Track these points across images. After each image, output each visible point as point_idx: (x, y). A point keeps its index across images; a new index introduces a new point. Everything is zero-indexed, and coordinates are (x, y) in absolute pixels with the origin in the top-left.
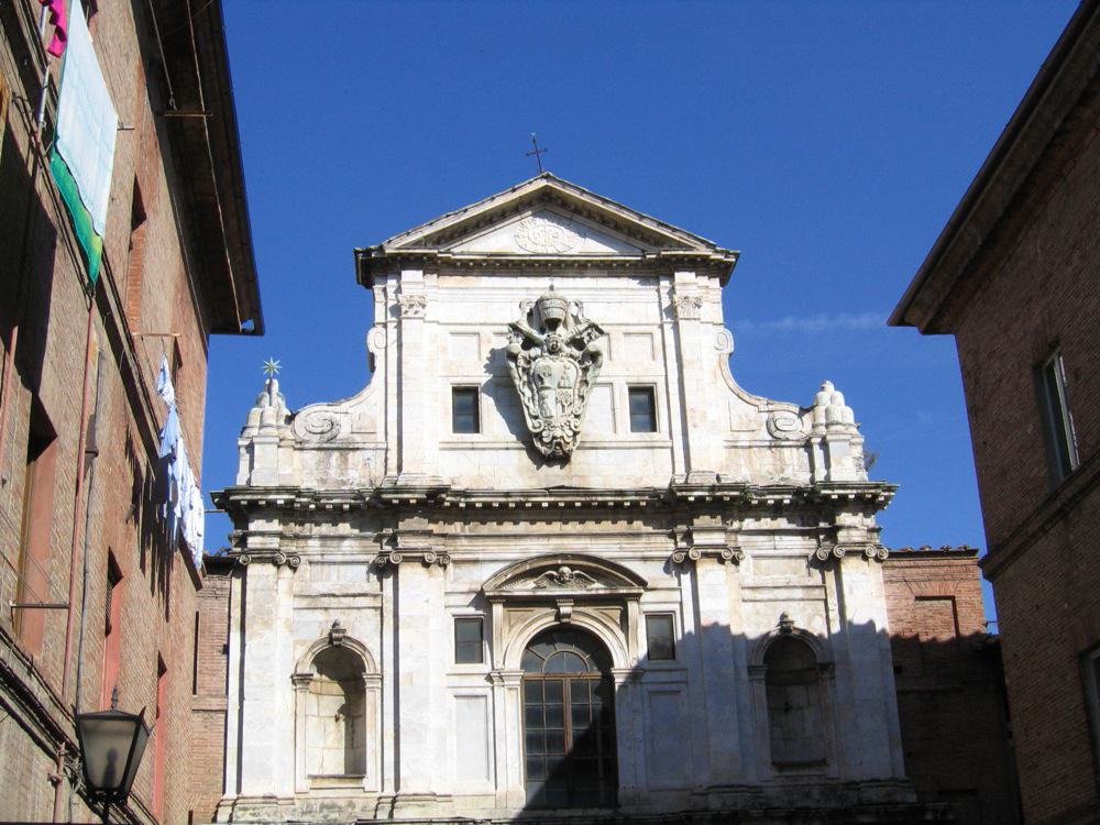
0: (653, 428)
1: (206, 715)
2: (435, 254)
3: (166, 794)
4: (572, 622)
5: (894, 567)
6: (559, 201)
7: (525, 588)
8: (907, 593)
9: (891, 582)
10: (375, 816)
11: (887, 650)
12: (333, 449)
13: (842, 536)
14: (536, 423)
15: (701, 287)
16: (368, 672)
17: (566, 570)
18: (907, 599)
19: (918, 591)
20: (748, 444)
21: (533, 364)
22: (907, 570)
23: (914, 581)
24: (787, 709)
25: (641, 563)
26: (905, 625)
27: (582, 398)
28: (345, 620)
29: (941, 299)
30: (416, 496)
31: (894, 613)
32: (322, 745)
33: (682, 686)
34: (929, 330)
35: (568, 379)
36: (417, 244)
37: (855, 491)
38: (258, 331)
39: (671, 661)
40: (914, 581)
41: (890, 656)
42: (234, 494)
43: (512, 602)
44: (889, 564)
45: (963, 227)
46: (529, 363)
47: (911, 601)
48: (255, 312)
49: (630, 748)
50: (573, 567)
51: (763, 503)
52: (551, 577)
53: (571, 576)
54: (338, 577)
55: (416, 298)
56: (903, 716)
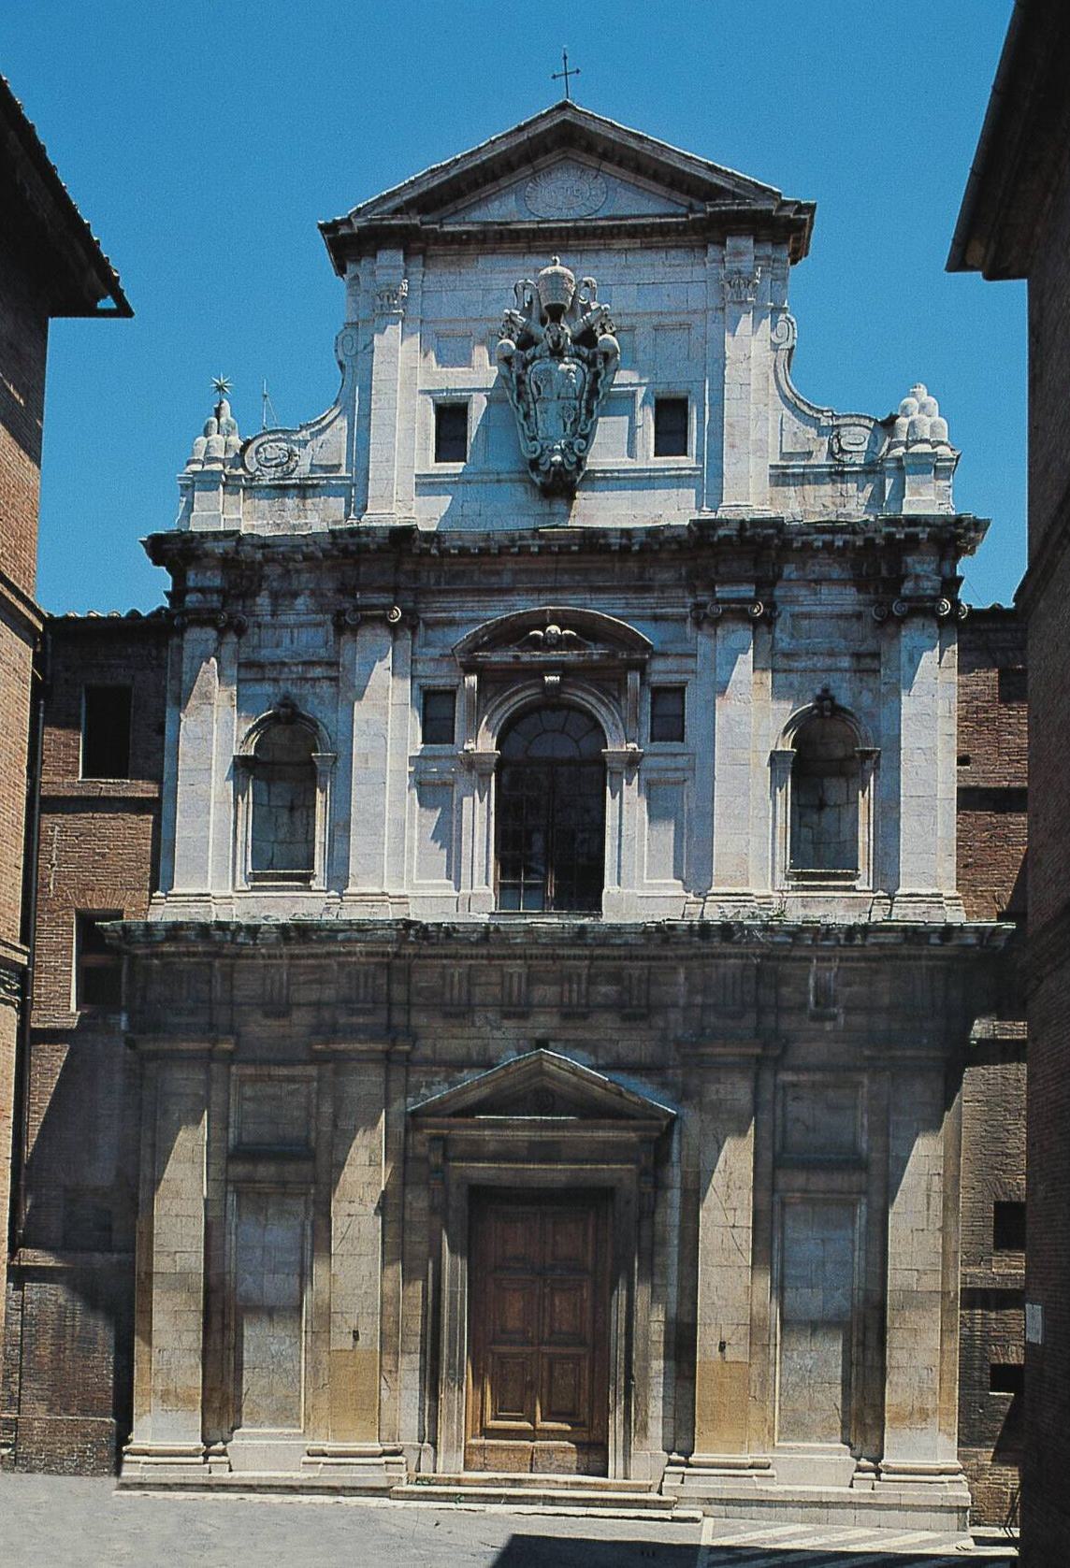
6: (583, 143)
10: (808, 1179)
13: (907, 588)
24: (821, 806)
25: (650, 626)
32: (272, 839)
39: (680, 743)
48: (113, 287)
51: (807, 546)
54: (292, 642)
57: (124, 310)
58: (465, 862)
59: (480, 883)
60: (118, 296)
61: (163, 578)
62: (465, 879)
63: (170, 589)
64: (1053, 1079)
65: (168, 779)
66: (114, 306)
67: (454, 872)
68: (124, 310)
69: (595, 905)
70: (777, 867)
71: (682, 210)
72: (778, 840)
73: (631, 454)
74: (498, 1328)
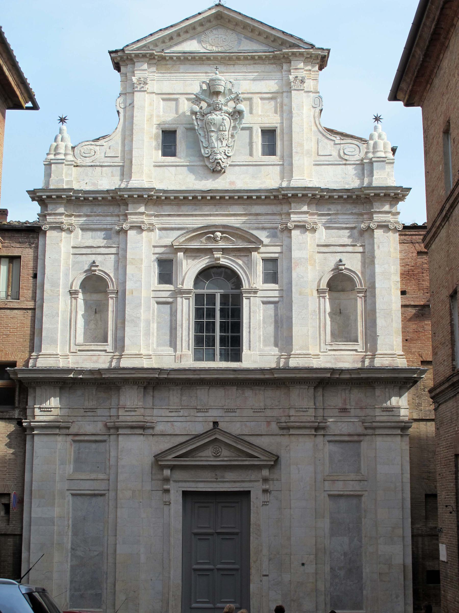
0: (248, 493)
3: (438, 429)
5: (406, 235)
7: (195, 245)
8: (413, 250)
9: (404, 243)
15: (306, 70)
16: (244, 288)
17: (219, 234)
18: (412, 253)
21: (205, 117)
22: (414, 237)
23: (417, 242)
26: (410, 268)
27: (233, 136)
28: (99, 259)
29: (410, 87)
31: (404, 261)
34: (408, 104)
35: (225, 126)
37: (384, 191)
38: (329, 50)
40: (417, 242)
42: (38, 192)
43: (186, 251)
44: (403, 233)
45: (413, 50)
47: (415, 254)
48: (30, 97)
50: (222, 233)
53: (221, 238)
55: (142, 79)
57: (35, 107)
58: (179, 340)
59: (185, 349)
60: (34, 102)
61: (36, 208)
62: (179, 347)
63: (39, 212)
64: (446, 447)
65: (38, 300)
66: (32, 106)
67: (173, 343)
68: (35, 107)
69: (237, 357)
70: (322, 341)
71: (271, 50)
72: (322, 329)
73: (251, 154)
74: (444, 568)
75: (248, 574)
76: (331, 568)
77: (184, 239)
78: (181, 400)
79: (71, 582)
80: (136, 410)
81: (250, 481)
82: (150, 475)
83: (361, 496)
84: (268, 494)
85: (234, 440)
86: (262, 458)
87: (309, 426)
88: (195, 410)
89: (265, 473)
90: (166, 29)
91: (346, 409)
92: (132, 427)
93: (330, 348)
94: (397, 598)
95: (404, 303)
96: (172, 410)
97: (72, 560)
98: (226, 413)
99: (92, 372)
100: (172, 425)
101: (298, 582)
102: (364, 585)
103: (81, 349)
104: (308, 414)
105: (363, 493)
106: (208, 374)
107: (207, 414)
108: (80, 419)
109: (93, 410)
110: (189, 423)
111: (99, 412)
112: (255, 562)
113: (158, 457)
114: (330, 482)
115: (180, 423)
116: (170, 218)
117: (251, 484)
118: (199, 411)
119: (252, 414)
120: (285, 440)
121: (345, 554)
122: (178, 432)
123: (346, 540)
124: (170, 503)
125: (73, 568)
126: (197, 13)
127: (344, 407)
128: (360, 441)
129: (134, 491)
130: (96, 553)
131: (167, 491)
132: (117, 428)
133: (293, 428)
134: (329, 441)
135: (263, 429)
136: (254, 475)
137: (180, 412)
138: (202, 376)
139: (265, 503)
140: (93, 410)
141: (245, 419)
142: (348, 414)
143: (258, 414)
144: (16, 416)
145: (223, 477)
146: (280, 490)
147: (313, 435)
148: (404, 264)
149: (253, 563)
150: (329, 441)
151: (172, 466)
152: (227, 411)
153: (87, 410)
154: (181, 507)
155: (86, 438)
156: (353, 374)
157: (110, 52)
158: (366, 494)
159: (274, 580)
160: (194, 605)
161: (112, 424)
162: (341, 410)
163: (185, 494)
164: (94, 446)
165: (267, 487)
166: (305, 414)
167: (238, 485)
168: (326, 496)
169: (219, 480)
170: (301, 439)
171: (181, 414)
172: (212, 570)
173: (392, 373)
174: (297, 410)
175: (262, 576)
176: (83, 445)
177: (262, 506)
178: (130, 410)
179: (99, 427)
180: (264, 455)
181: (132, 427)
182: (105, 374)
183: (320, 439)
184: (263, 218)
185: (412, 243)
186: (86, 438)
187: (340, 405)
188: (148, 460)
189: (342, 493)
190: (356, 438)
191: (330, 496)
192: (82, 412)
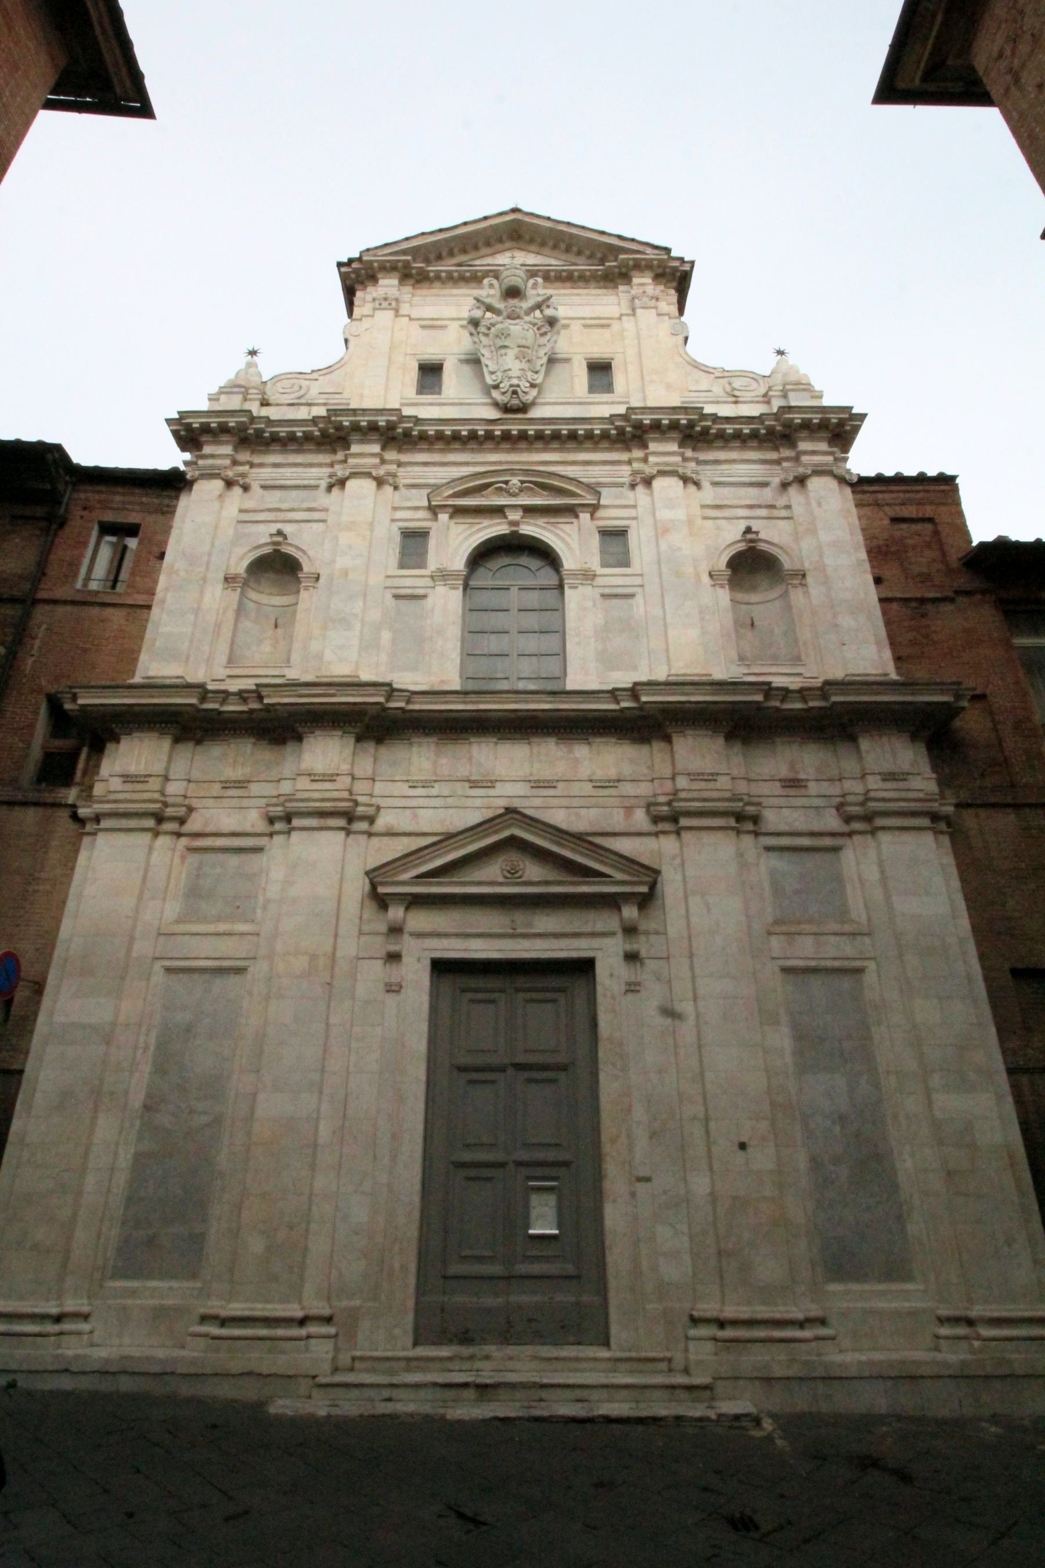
0: (585, 967)
1: (129, 610)
2: (408, 262)
4: (521, 532)
5: (864, 492)
11: (864, 560)
12: (301, 404)
14: (494, 377)
18: (881, 520)
19: (891, 512)
20: (313, 1329)
22: (880, 496)
23: (887, 504)
30: (367, 418)
33: (639, 590)
36: (391, 254)
37: (819, 416)
38: (692, 263)
41: (867, 566)
46: (489, 329)
49: (579, 644)
52: (500, 489)
56: (888, 623)
75: (599, 1176)
76: (813, 1159)
77: (451, 492)
78: (435, 763)
79: (130, 1201)
80: (335, 778)
81: (593, 935)
82: (357, 921)
83: (860, 971)
84: (638, 964)
85: (554, 838)
86: (619, 876)
87: (721, 809)
88: (467, 785)
89: (630, 912)
90: (432, 233)
91: (798, 780)
92: (322, 814)
93: (746, 671)
94: (1009, 1246)
95: (883, 595)
96: (415, 784)
97: (140, 1139)
98: (534, 790)
99: (245, 695)
100: (415, 816)
101: (735, 1198)
102: (905, 1207)
103: (232, 673)
104: (718, 785)
105: (866, 963)
106: (495, 702)
107: (492, 792)
108: (210, 802)
109: (241, 785)
110: (451, 811)
111: (255, 789)
112: (613, 1141)
113: (375, 876)
114: (782, 937)
115: (431, 811)
116: (426, 469)
117: (596, 943)
118: (474, 784)
119: (594, 792)
120: (668, 844)
121: (842, 1119)
122: (426, 829)
123: (840, 1081)
124: (401, 987)
125: (140, 1160)
126: (481, 216)
127: (791, 776)
128: (836, 849)
129: (313, 957)
130: (205, 1119)
131: (394, 957)
132: (288, 818)
133: (689, 814)
134: (768, 849)
135: (617, 820)
136: (605, 921)
137: (433, 787)
138: (482, 707)
139: (633, 988)
140: (241, 784)
141: (576, 802)
142: (803, 792)
143: (606, 792)
144: (70, 801)
145: (530, 925)
146: (665, 955)
147: (732, 828)
148: (869, 537)
149: (609, 1145)
150: (768, 849)
151: (409, 897)
152: (538, 785)
153: (228, 785)
154: (425, 998)
155: (220, 842)
156: (813, 700)
157: (340, 265)
158: (872, 966)
159: (665, 1192)
160: (455, 1269)
161: (280, 809)
162: (787, 784)
163: (441, 967)
164: (234, 860)
165: (635, 947)
166: (711, 785)
167: (564, 943)
168: (777, 970)
169: (519, 931)
170: (707, 838)
171: (434, 792)
172: (502, 1165)
173: (900, 694)
174: (692, 777)
175: (634, 1179)
176: (210, 857)
177: (625, 994)
178: (321, 778)
179: (252, 820)
180: (622, 870)
181: (322, 814)
182: (269, 696)
183: (748, 840)
184: (597, 468)
185: (878, 505)
186: (220, 842)
187: (784, 772)
188: (357, 887)
189: (813, 963)
190: (827, 842)
191: (786, 970)
192: (216, 789)
